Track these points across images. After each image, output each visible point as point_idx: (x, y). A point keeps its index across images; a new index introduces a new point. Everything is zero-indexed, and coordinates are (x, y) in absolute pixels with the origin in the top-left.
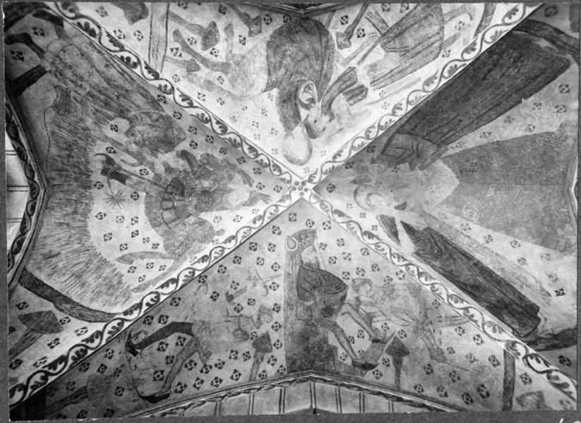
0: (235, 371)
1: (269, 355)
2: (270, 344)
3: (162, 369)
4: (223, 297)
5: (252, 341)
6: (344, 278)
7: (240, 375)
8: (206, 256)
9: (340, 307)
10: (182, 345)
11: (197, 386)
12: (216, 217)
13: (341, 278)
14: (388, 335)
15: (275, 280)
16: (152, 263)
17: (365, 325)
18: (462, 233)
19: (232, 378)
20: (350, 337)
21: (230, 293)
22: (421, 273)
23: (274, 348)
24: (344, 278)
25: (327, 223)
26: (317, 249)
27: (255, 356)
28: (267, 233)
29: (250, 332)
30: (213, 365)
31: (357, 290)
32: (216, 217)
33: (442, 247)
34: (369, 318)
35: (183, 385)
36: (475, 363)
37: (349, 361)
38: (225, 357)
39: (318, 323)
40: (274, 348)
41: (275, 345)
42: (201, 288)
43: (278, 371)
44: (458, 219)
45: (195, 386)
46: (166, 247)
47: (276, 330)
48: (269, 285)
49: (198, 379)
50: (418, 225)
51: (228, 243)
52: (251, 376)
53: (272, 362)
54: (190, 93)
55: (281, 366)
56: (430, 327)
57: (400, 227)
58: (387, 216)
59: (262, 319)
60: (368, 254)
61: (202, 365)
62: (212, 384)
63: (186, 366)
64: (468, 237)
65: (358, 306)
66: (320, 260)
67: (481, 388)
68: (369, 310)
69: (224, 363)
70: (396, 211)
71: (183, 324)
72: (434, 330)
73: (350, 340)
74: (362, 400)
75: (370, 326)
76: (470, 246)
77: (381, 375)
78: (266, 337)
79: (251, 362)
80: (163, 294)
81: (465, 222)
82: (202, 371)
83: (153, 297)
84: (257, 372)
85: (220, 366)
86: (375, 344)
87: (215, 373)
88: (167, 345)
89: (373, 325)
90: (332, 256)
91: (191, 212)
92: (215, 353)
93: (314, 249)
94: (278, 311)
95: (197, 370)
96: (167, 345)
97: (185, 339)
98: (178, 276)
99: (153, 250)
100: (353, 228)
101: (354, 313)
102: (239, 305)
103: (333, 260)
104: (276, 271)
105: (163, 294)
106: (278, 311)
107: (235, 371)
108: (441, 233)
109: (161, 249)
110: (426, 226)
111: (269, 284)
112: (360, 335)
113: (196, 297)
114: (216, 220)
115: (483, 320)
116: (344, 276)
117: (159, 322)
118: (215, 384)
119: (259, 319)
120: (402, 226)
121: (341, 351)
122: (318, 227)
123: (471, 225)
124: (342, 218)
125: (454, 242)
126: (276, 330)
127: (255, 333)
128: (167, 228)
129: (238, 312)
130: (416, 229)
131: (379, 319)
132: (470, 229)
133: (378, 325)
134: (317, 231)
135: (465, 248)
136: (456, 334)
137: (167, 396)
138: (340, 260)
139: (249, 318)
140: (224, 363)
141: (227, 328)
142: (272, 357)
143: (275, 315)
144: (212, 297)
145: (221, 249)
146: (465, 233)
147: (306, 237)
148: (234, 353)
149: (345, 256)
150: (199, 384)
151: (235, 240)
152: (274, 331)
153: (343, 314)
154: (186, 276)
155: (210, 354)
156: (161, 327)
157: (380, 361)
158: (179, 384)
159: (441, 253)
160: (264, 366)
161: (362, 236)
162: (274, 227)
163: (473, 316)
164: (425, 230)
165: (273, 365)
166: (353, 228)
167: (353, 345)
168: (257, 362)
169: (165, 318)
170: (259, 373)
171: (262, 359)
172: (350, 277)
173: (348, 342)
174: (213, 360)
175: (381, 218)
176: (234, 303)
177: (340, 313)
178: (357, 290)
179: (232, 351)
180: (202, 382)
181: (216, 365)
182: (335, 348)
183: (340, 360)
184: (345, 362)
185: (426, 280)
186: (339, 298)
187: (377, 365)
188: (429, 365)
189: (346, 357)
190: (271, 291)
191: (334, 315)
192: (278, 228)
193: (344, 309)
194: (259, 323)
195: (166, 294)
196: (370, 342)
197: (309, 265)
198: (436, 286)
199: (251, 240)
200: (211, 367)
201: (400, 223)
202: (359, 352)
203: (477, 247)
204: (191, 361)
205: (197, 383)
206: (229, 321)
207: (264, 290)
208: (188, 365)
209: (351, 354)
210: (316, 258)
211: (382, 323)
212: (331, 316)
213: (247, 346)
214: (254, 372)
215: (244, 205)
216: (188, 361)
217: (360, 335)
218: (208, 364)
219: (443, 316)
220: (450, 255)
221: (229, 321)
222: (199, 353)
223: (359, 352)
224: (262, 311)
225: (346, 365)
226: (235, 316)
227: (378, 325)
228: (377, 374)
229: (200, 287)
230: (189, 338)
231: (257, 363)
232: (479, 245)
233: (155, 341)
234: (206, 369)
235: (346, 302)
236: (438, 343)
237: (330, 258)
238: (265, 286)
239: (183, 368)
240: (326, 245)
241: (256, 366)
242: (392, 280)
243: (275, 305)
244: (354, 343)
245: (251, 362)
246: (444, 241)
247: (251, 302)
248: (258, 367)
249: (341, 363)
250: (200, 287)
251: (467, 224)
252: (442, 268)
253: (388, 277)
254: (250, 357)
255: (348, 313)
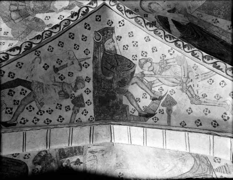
0: (60, 117)
1: (83, 109)
2: (84, 102)
3: (11, 107)
4: (51, 68)
5: (72, 99)
6: (133, 59)
7: (63, 119)
8: (39, 35)
9: (131, 79)
10: (24, 95)
11: (35, 122)
12: (46, 17)
13: (131, 60)
14: (163, 94)
15: (87, 61)
16: (4, 43)
17: (147, 90)
18: (213, 25)
19: (58, 120)
20: (137, 99)
21: (56, 67)
22: (185, 45)
23: (86, 105)
24: (133, 59)
25: (122, 22)
26: (115, 40)
27: (73, 109)
28: (80, 26)
29: (70, 94)
30: (45, 111)
31: (142, 67)
32: (46, 17)
33: (200, 34)
34: (150, 85)
35: (25, 120)
36: (220, 100)
37: (136, 114)
38: (53, 107)
39: (115, 91)
40: (86, 105)
41: (86, 103)
42: (37, 60)
43: (89, 119)
44: (210, 16)
45: (33, 121)
46: (13, 34)
47: (88, 94)
48: (82, 64)
49: (35, 118)
50: (183, 22)
51: (54, 29)
52: (71, 120)
53: (84, 113)
54: (28, 142)
55: (91, 116)
56: (191, 84)
57: (171, 23)
58: (162, 16)
59: (78, 86)
60: (150, 40)
61: (38, 110)
62: (45, 122)
63: (27, 108)
64: (217, 27)
65: (142, 78)
66: (117, 48)
67: (224, 115)
68: (149, 79)
69: (52, 111)
70: (168, 14)
71: (25, 81)
72: (193, 85)
73: (138, 100)
74: (145, 133)
75: (151, 90)
76: (218, 32)
77: (158, 119)
78: (81, 96)
79: (70, 112)
80: (11, 55)
81: (214, 18)
82: (38, 114)
83: (4, 56)
84: (75, 119)
85: (50, 112)
86: (154, 101)
87: (46, 116)
88: (14, 92)
89: (153, 89)
90: (125, 44)
91: (30, 13)
92: (47, 104)
93: (113, 41)
94: (88, 82)
95: (34, 113)
96: (14, 92)
97: (26, 92)
98: (21, 45)
99: (5, 36)
100: (139, 21)
101: (140, 83)
102: (62, 75)
103: (126, 47)
104: (87, 54)
105: (11, 55)
106: (88, 82)
107: (60, 117)
108: (199, 25)
109: (10, 35)
110: (189, 22)
111: (82, 63)
112: (144, 97)
113: (33, 65)
114: (46, 18)
115: (226, 68)
116: (133, 58)
117: (9, 76)
118: (47, 122)
119: (76, 86)
120: (172, 22)
121: (131, 108)
122: (115, 25)
123: (219, 20)
124: (131, 15)
125: (207, 30)
126: (88, 94)
127: (73, 94)
128: (14, 23)
129: (62, 80)
130: (182, 24)
131: (157, 84)
132: (218, 22)
133: (156, 89)
134: (115, 28)
135: (216, 34)
136: (208, 84)
137: (15, 124)
138: (131, 47)
139: (69, 85)
140: (52, 111)
141: (55, 89)
142: (85, 110)
143: (86, 83)
144: (44, 67)
145: (50, 32)
146: (215, 24)
147: (108, 32)
148: (59, 106)
149: (134, 43)
150: (36, 121)
151: (59, 28)
152: (86, 94)
153: (133, 84)
154: (26, 46)
155: (43, 104)
156: (10, 80)
157: (158, 111)
158: (23, 119)
159: (199, 37)
160: (79, 115)
161: (146, 26)
162: (86, 24)
163: (219, 66)
164: (188, 24)
165: (85, 115)
166: (139, 21)
167: (139, 103)
168: (75, 113)
169: (12, 74)
170: (76, 119)
171: (78, 111)
172: (137, 58)
173: (136, 101)
174: (46, 108)
175: (158, 17)
176: (59, 74)
177: (131, 83)
178: (142, 67)
179: (58, 104)
180: (38, 120)
181: (47, 111)
182: (127, 106)
183: (130, 113)
184: (134, 114)
185: (188, 49)
186: (130, 73)
187: (155, 114)
188: (190, 108)
189: (135, 111)
190: (84, 68)
191: (126, 85)
192: (89, 25)
193: (134, 80)
194: (76, 89)
195: (13, 55)
196: (151, 100)
197: (110, 52)
198: (195, 52)
199: (70, 31)
200: (44, 112)
201: (171, 21)
202: (143, 107)
203: (223, 33)
204: (30, 106)
205: (34, 120)
206: (56, 85)
207: (79, 67)
208: (29, 108)
209: (138, 109)
210: (114, 46)
211: (159, 87)
212: (125, 86)
213: (67, 102)
214: (73, 118)
215: (65, 9)
216: (28, 106)
217: (144, 97)
218: (42, 109)
219: (200, 74)
220: (205, 37)
221: (56, 85)
222: (36, 102)
223: (143, 107)
224: (78, 80)
225: (135, 116)
226: (59, 82)
227: (156, 89)
228: (155, 119)
229: (36, 58)
230: (29, 91)
231: (75, 112)
232: (224, 31)
233: (6, 88)
234: (41, 112)
235: (134, 76)
236: (196, 93)
237: (124, 46)
238: (80, 64)
239: (25, 109)
240: (121, 37)
241: (74, 115)
242: (165, 56)
243: (87, 77)
244: (140, 102)
245: (70, 112)
246: (201, 30)
247: (70, 74)
248: (76, 116)
249: (131, 115)
250: (36, 58)
251: (216, 19)
252: (198, 45)
253: (163, 55)
254: (70, 109)
255: (136, 83)
